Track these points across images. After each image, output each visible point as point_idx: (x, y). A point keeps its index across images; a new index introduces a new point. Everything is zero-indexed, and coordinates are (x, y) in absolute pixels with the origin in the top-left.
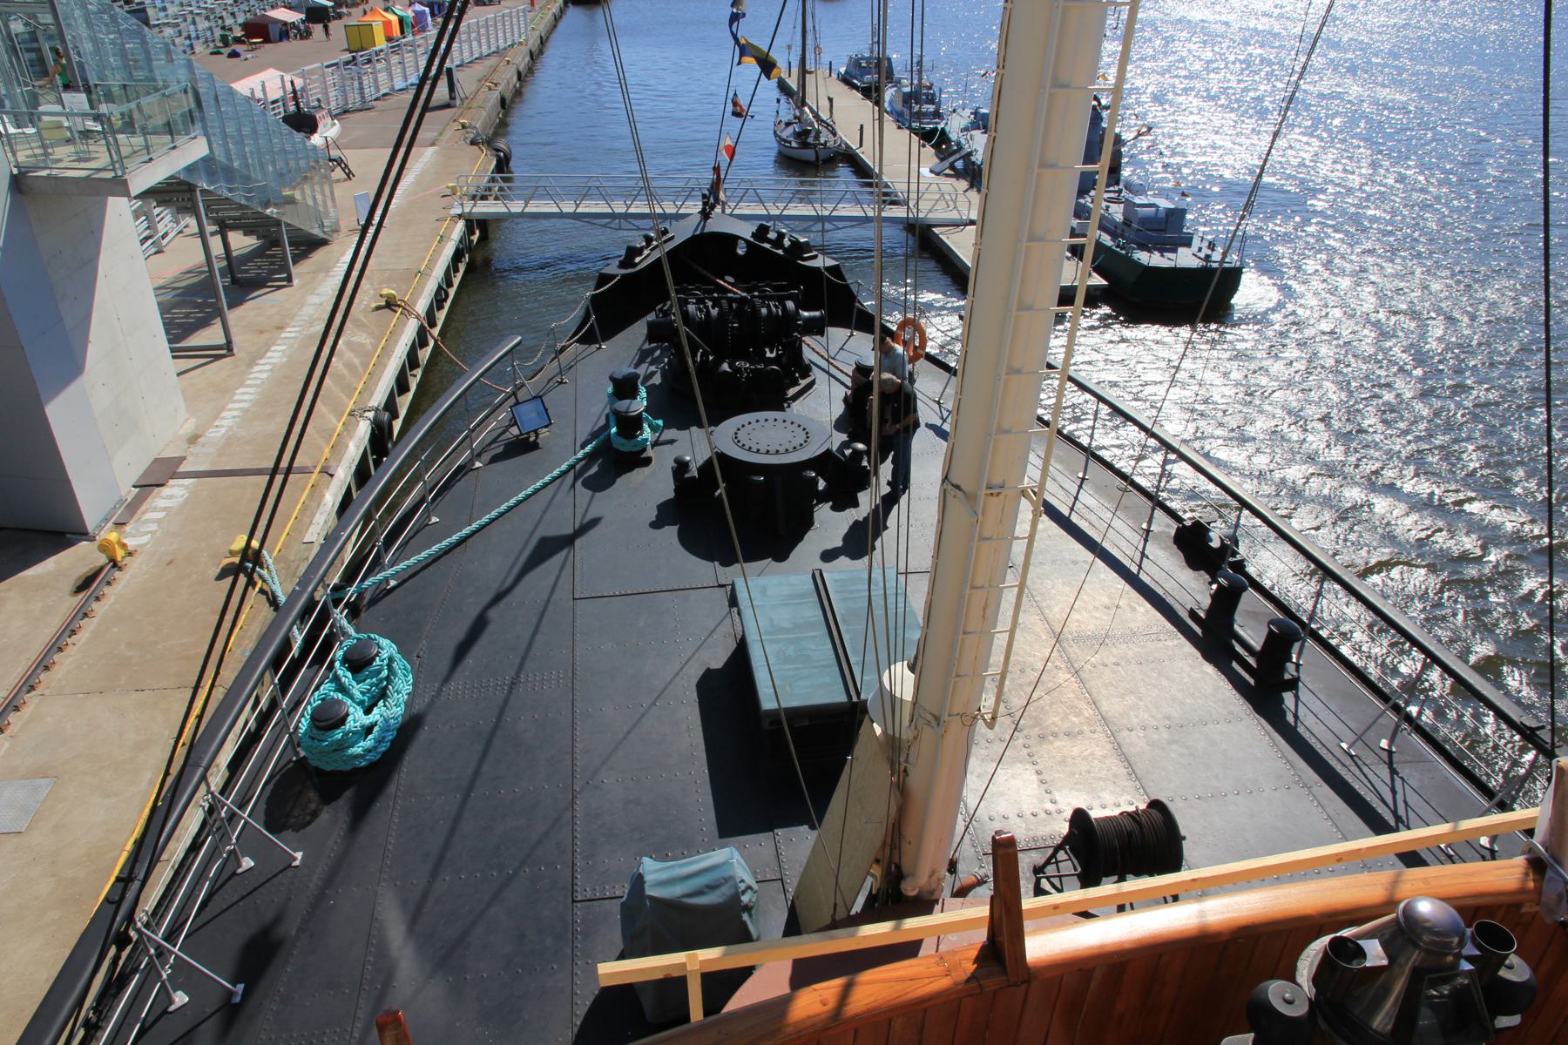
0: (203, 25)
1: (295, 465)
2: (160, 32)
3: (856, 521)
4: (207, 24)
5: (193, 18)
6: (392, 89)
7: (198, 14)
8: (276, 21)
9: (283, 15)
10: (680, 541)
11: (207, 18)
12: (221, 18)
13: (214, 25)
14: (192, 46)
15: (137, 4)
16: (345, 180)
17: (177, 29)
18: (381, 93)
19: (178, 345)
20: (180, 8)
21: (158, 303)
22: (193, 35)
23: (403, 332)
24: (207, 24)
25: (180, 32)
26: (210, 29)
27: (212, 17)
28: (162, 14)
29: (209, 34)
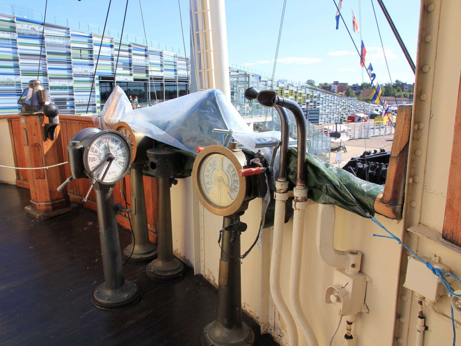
0: (336, 116)
1: (88, 110)
2: (322, 116)
3: (241, 234)
4: (337, 116)
5: (333, 114)
6: (380, 135)
7: (335, 113)
8: (358, 116)
9: (362, 115)
10: (244, 214)
11: (338, 114)
12: (342, 115)
13: (339, 116)
14: (330, 121)
15: (317, 108)
16: (344, 153)
17: (327, 116)
18: (375, 135)
19: (341, 198)
20: (330, 111)
21: (160, 103)
22: (332, 118)
23: (452, 243)
24: (337, 116)
25: (328, 116)
26: (338, 117)
27: (339, 114)
28: (324, 112)
29: (337, 118)
